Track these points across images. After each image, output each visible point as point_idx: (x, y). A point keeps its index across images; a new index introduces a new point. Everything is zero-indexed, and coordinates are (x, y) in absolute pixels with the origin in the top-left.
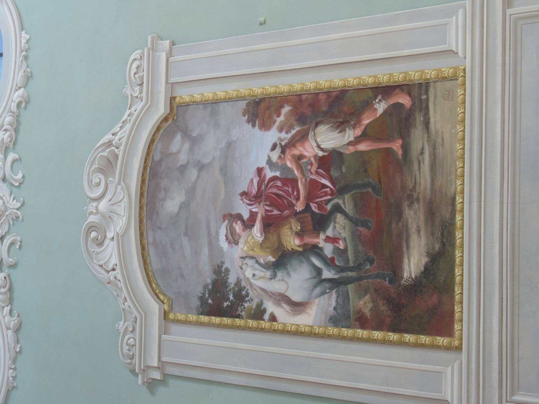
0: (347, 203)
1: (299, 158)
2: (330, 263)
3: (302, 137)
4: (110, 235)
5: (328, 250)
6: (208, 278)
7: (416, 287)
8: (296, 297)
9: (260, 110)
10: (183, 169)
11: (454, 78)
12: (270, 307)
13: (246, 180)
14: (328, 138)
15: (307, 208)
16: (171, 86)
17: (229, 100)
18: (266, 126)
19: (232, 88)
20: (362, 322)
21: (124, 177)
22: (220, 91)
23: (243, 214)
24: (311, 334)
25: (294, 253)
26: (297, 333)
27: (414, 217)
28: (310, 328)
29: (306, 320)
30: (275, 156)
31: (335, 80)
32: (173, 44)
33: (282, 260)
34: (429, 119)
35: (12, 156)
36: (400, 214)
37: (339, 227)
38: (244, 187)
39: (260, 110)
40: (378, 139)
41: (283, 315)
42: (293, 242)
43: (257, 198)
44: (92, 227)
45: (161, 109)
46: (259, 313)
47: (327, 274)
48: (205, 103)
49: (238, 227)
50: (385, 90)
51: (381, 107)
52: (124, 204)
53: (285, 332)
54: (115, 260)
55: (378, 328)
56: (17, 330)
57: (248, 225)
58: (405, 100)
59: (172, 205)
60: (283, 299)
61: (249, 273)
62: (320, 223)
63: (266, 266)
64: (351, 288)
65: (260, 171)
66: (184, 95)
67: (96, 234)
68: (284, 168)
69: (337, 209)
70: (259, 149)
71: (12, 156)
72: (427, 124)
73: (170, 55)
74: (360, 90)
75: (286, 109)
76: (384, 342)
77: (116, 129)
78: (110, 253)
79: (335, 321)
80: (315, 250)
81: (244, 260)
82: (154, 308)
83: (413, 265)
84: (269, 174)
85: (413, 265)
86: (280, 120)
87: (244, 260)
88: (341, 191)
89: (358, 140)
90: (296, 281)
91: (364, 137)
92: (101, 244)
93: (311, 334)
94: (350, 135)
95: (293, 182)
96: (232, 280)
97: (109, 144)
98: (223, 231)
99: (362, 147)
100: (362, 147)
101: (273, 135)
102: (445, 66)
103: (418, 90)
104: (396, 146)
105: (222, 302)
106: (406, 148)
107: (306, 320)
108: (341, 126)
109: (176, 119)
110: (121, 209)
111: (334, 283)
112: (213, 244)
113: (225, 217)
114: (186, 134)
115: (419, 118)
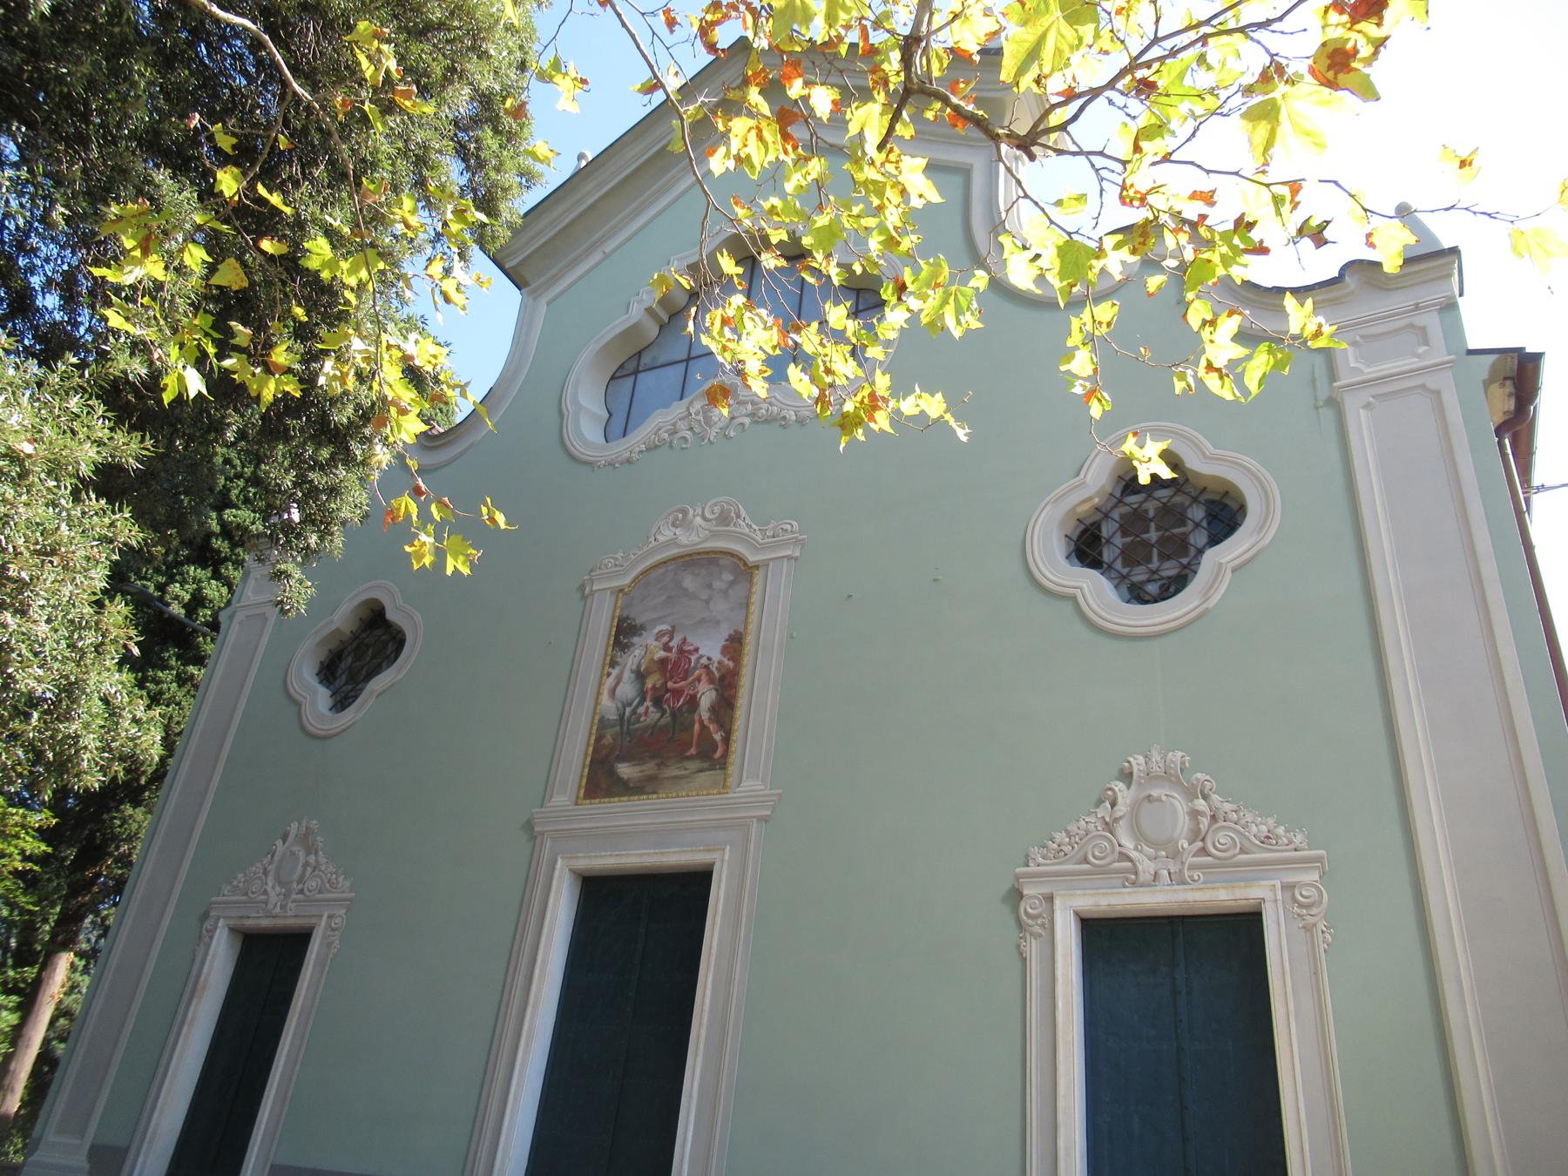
0: (667, 719)
1: (699, 679)
2: (634, 712)
3: (711, 681)
4: (678, 531)
5: (641, 710)
6: (638, 622)
7: (612, 773)
8: (618, 691)
9: (735, 645)
10: (710, 586)
11: (724, 787)
12: (615, 672)
13: (694, 640)
15: (668, 690)
16: (766, 564)
17: (746, 623)
18: (725, 651)
19: (752, 628)
21: (714, 535)
22: (754, 618)
24: (597, 703)
25: (643, 684)
26: (599, 693)
27: (650, 767)
28: (253, 394)
29: (605, 699)
30: (704, 661)
31: (740, 713)
32: (796, 559)
33: (640, 676)
35: (747, 421)
36: (652, 757)
37: (654, 715)
38: (689, 640)
39: (735, 645)
40: (700, 734)
41: (610, 682)
42: (649, 684)
43: (681, 651)
44: (685, 512)
45: (752, 558)
46: (613, 664)
47: (628, 710)
48: (748, 597)
49: (666, 639)
50: (727, 740)
51: (717, 737)
52: (697, 539)
53: (600, 684)
54: (661, 538)
55: (595, 751)
56: (629, 461)
57: (667, 648)
59: (689, 582)
60: (619, 679)
61: (637, 652)
62: (658, 702)
63: (639, 665)
64: (618, 729)
65: (696, 650)
66: (758, 577)
67: (682, 522)
68: (695, 668)
70: (710, 649)
71: (747, 421)
72: (701, 770)
73: (789, 558)
74: (731, 720)
75: (731, 664)
76: (586, 754)
77: (748, 521)
78: (666, 534)
79: (602, 720)
80: (643, 700)
82: (626, 581)
83: (625, 770)
84: (693, 658)
85: (625, 770)
86: (726, 661)
88: (673, 715)
89: (701, 722)
90: (627, 690)
91: (703, 727)
92: (673, 525)
93: (597, 703)
94: (705, 715)
95: (685, 678)
96: (635, 640)
97: (738, 516)
98: (665, 627)
99: (697, 726)
100: (697, 726)
101: (716, 656)
102: (731, 781)
103: (722, 764)
104: (693, 751)
105: (624, 632)
106: (691, 758)
107: (605, 699)
108: (713, 709)
109: (745, 571)
110: (694, 538)
111: (622, 716)
112: (659, 620)
113: (673, 627)
114: (732, 583)
115: (705, 765)
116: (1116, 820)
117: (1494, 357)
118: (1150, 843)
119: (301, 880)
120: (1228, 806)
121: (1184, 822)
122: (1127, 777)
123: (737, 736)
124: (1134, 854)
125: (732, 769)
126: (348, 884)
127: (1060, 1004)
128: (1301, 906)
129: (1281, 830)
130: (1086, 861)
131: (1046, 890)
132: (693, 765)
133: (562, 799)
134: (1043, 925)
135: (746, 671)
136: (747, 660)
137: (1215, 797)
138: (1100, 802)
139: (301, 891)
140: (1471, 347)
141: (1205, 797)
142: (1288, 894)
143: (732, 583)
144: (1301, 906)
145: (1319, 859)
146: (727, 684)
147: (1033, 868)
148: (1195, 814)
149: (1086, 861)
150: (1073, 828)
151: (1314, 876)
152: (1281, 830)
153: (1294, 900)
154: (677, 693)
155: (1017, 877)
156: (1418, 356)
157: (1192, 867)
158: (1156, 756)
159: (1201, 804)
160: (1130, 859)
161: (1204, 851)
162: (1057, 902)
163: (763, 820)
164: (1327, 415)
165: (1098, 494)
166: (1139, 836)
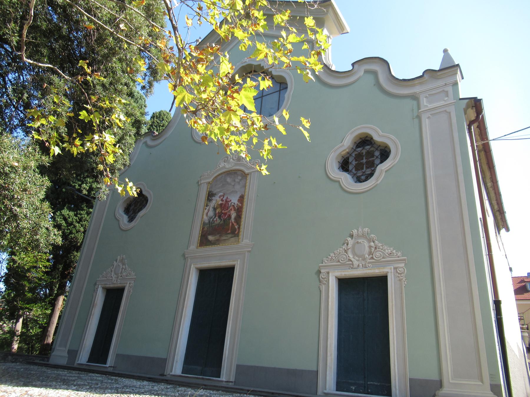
1: (231, 210)
2: (213, 220)
3: (235, 210)
9: (241, 199)
10: (234, 181)
12: (207, 208)
13: (230, 198)
14: (233, 215)
20: (203, 229)
21: (236, 165)
22: (247, 190)
23: (502, 302)
24: (202, 218)
26: (203, 215)
27: (217, 237)
30: (233, 204)
31: (243, 220)
34: (241, 215)
39: (241, 199)
40: (232, 227)
41: (206, 211)
43: (226, 201)
45: (247, 172)
46: (207, 206)
48: (246, 184)
49: (222, 197)
50: (239, 228)
51: (236, 227)
53: (203, 212)
58: (236, 232)
59: (229, 180)
60: (209, 210)
69: (221, 220)
70: (234, 200)
72: (232, 237)
75: (240, 205)
81: (217, 200)
84: (230, 203)
85: (210, 238)
87: (217, 200)
89: (232, 223)
90: (211, 213)
93: (202, 218)
94: (233, 221)
99: (231, 224)
100: (231, 224)
101: (236, 202)
103: (238, 235)
104: (229, 231)
105: (210, 196)
106: (229, 233)
107: (205, 217)
108: (235, 219)
111: (209, 221)
112: (220, 192)
116: (348, 249)
117: (467, 100)
118: (358, 256)
119: (370, 253)
120: (380, 244)
121: (367, 249)
122: (352, 236)
123: (242, 227)
124: (353, 259)
125: (241, 237)
126: (399, 254)
127: (330, 304)
128: (399, 274)
129: (394, 251)
130: (339, 261)
131: (327, 270)
132: (230, 236)
133: (193, 247)
134: (326, 281)
135: (245, 207)
136: (245, 203)
137: (376, 242)
138: (344, 244)
139: (121, 276)
140: (461, 97)
141: (373, 242)
142: (395, 270)
143: (241, 180)
144: (399, 274)
145: (405, 260)
146: (239, 211)
147: (324, 264)
148: (370, 247)
149: (339, 261)
150: (336, 252)
151: (403, 265)
152: (394, 251)
153: (397, 272)
154: (225, 214)
155: (320, 267)
156: (445, 101)
157: (369, 263)
158: (360, 230)
159: (124, 267)
160: (351, 261)
161: (372, 258)
162: (330, 274)
163: (249, 251)
164: (416, 120)
165: (348, 148)
166: (354, 254)
